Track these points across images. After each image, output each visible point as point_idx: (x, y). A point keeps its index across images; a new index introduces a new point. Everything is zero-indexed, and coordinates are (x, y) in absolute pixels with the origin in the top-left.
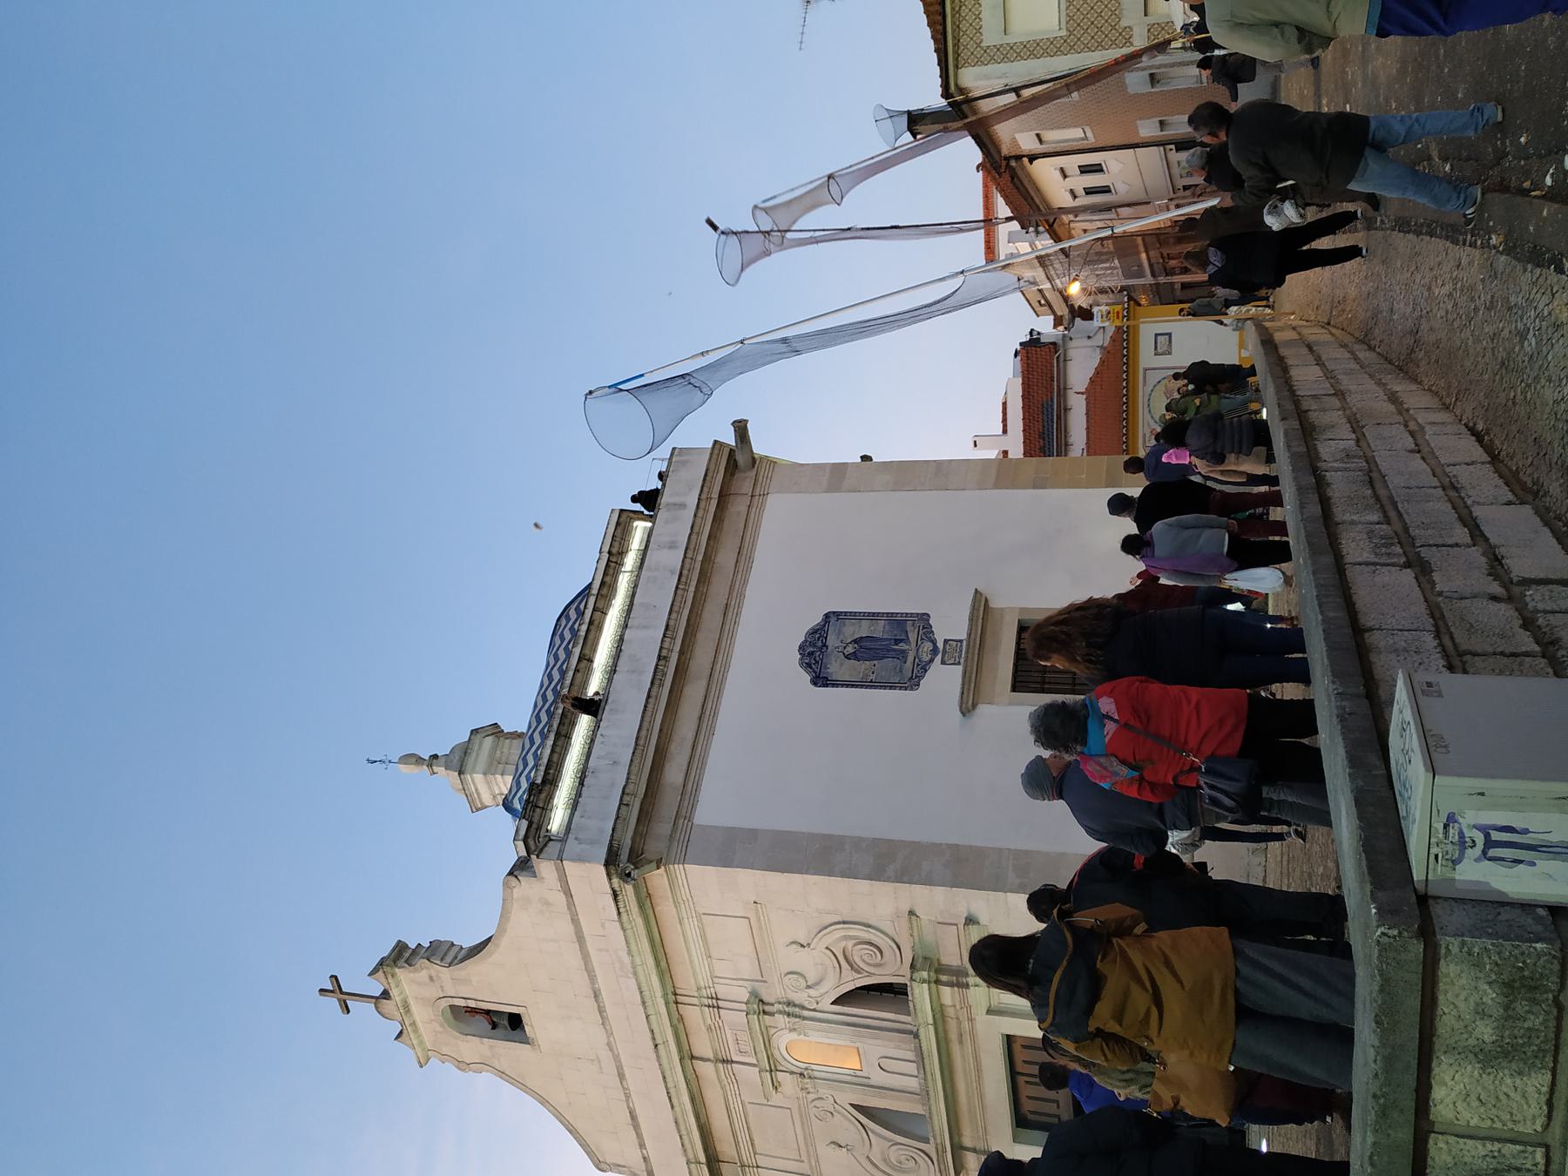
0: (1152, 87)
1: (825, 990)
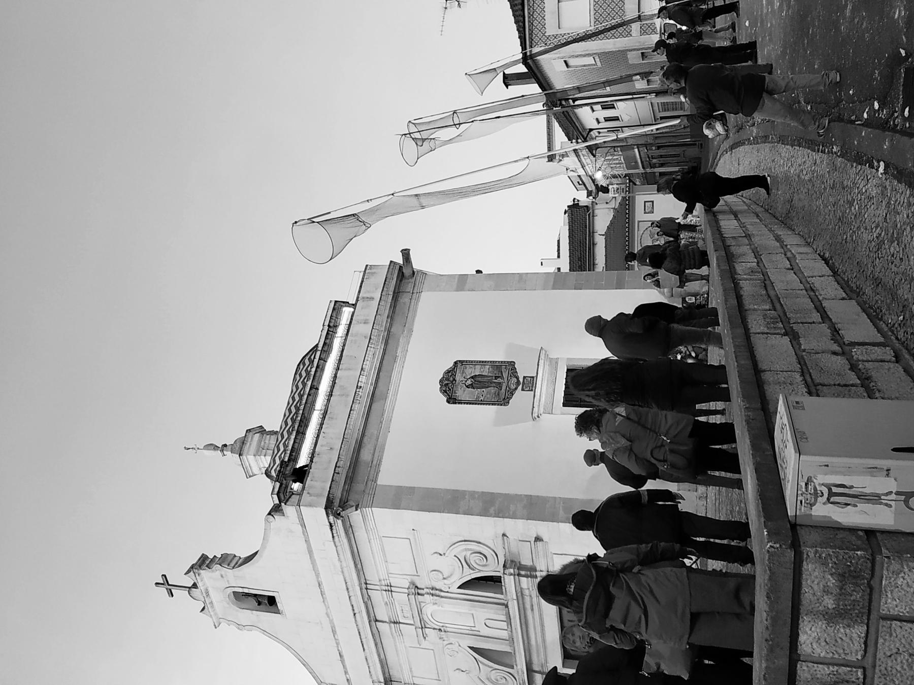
0: (643, 60)
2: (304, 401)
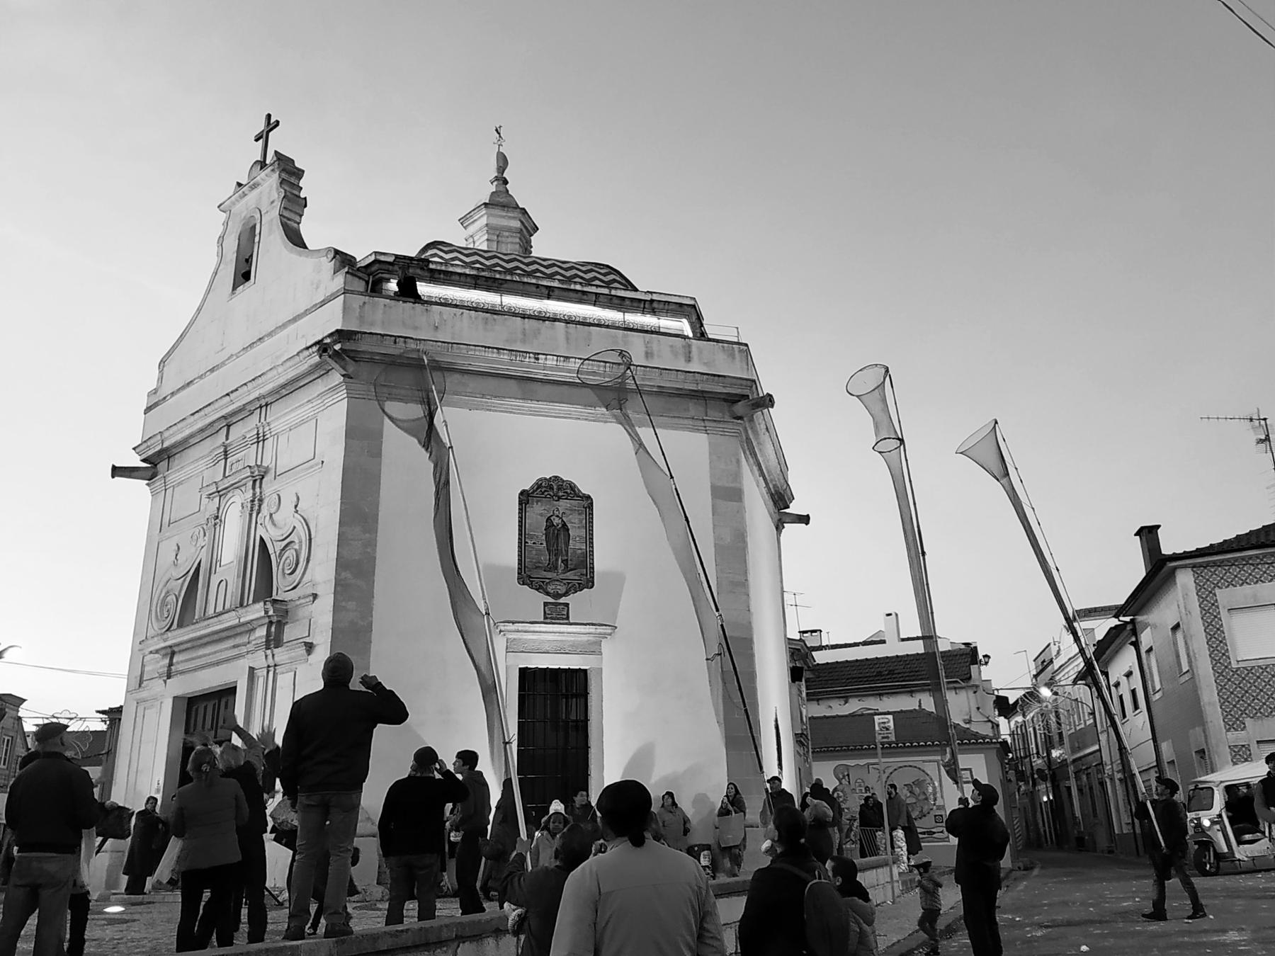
0: (1196, 752)
1: (269, 530)
2: (525, 280)
